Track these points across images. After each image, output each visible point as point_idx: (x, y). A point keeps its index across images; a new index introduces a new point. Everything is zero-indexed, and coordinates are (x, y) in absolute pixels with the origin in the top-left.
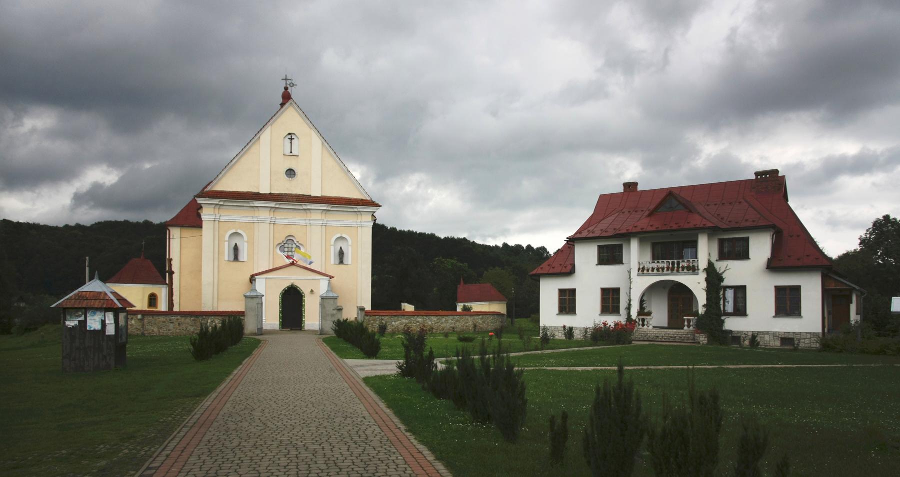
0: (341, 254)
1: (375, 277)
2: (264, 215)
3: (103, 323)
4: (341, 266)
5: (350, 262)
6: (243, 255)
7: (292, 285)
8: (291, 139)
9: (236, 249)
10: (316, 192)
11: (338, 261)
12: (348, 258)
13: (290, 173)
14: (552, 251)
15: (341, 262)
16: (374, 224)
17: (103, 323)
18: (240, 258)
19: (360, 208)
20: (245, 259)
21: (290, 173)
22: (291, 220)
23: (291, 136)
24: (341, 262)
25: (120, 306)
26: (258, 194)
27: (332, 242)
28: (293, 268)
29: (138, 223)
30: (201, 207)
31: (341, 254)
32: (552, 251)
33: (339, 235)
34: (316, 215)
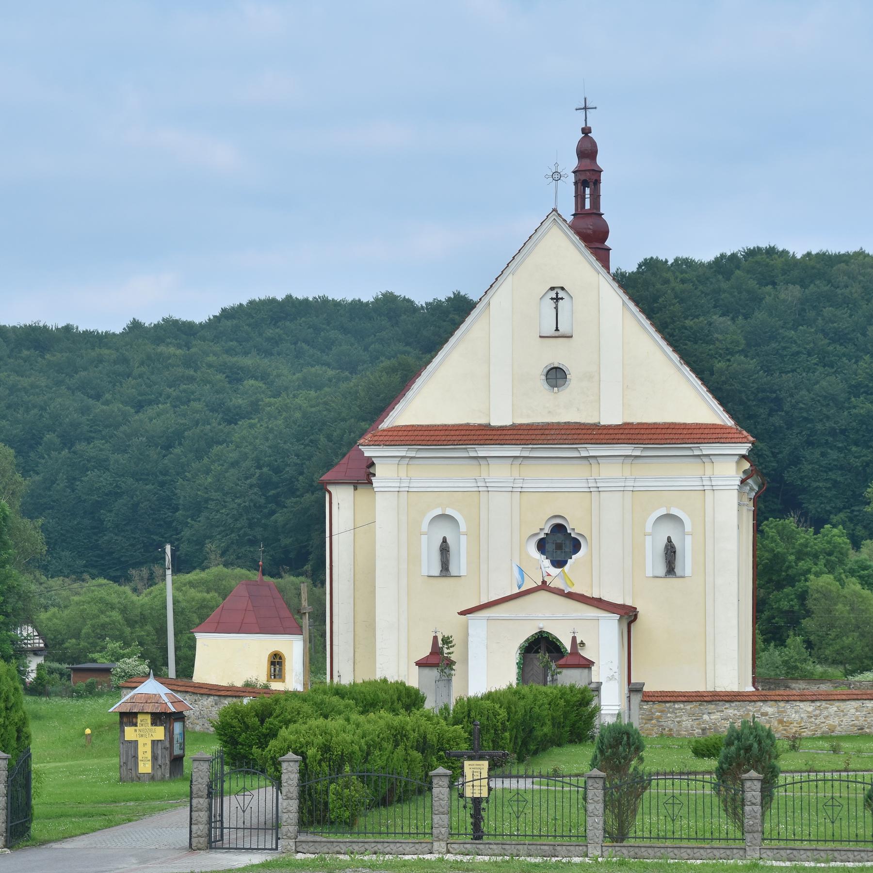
0: (670, 553)
2: (499, 474)
3: (276, 661)
4: (672, 581)
5: (688, 572)
6: (460, 563)
7: (541, 632)
8: (557, 299)
9: (444, 549)
11: (661, 569)
12: (687, 562)
15: (671, 570)
16: (184, 722)
17: (276, 661)
18: (453, 570)
20: (463, 572)
21: (556, 376)
23: (557, 294)
24: (671, 570)
25: (173, 710)
26: (487, 428)
28: (543, 595)
29: (357, 307)
31: (670, 553)
33: (663, 511)
34: (613, 468)
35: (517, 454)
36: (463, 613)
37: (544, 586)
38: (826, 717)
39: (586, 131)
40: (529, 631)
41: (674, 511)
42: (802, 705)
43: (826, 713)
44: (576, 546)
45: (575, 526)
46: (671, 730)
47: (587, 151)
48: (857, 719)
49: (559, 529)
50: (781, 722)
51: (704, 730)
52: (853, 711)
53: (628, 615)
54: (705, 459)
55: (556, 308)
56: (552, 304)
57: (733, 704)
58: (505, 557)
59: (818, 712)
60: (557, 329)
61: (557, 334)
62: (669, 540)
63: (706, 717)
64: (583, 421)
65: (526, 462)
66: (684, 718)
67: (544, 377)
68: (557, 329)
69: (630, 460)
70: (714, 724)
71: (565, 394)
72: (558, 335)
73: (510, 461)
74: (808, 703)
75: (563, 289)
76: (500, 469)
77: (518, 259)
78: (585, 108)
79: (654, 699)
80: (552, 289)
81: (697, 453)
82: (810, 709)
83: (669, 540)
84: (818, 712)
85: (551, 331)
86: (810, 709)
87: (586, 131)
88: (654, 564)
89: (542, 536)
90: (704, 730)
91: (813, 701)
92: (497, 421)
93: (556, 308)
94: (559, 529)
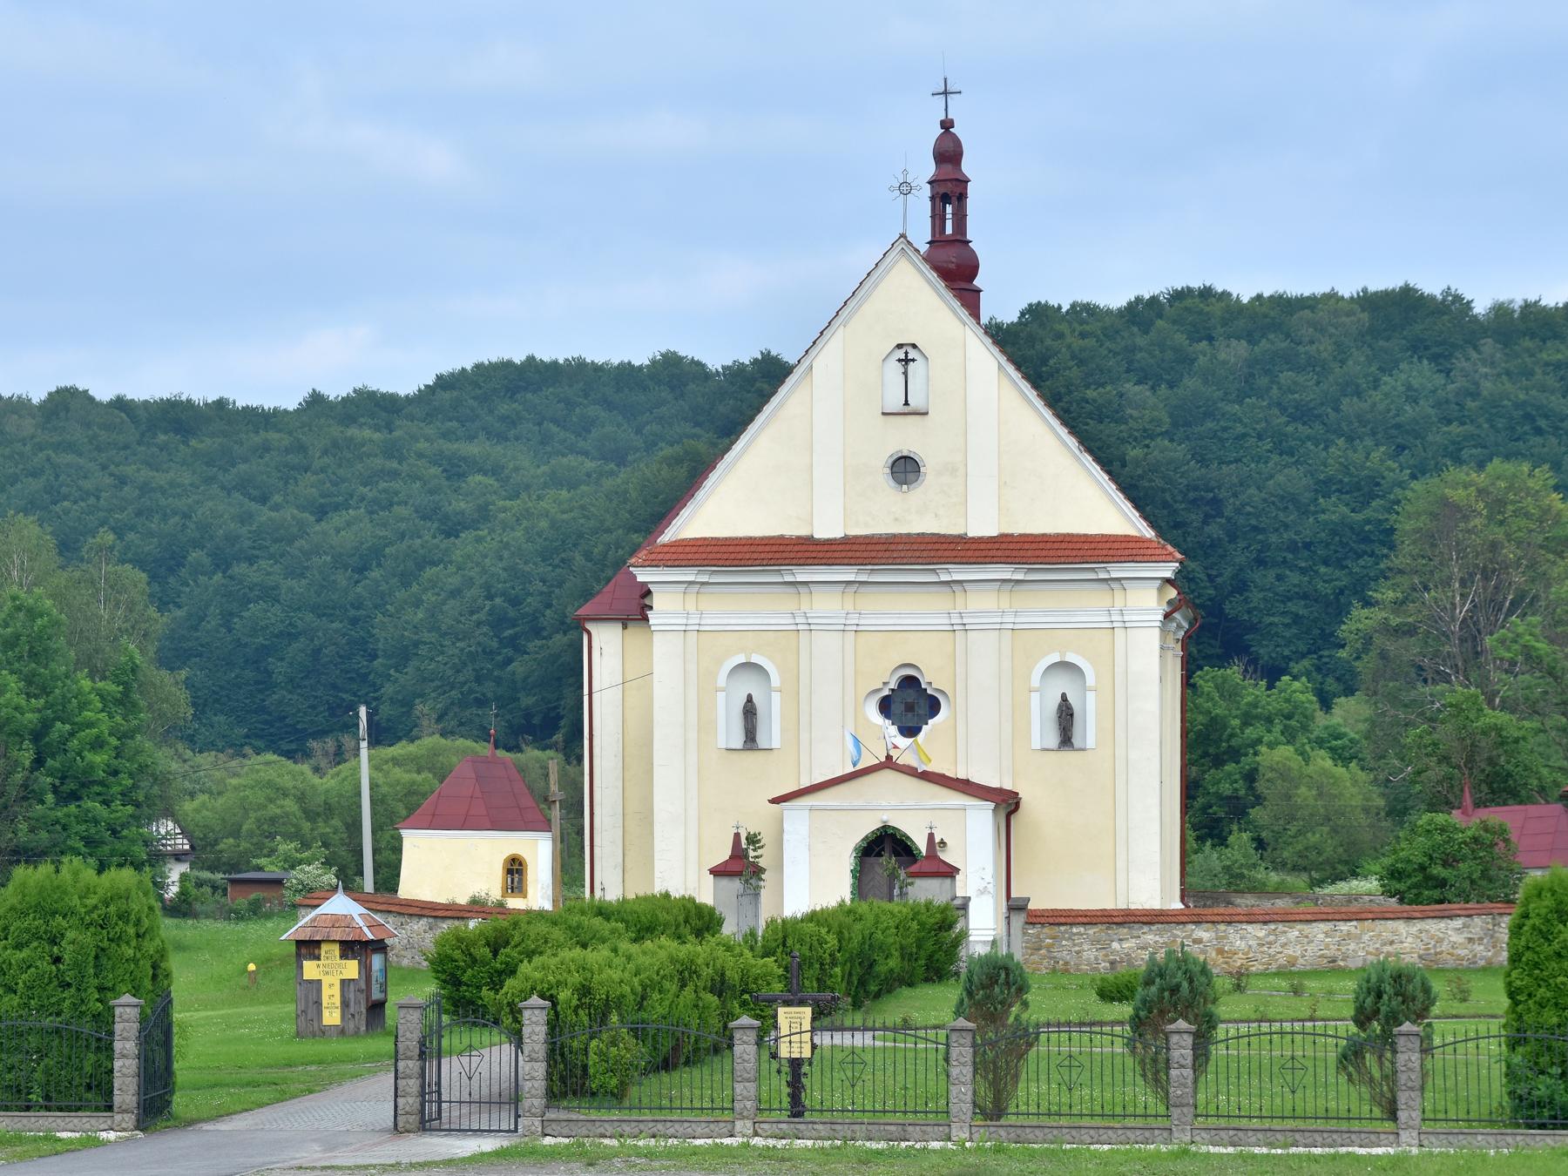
0: (1066, 716)
1: (1009, 350)
2: (826, 606)
3: (515, 869)
4: (1068, 756)
6: (772, 731)
8: (906, 361)
9: (750, 711)
10: (983, 526)
11: (1053, 739)
12: (1089, 729)
13: (905, 469)
14: (35, 401)
15: (1066, 740)
17: (515, 869)
18: (762, 740)
19: (1117, 571)
21: (905, 469)
22: (907, 624)
23: (906, 354)
24: (1066, 740)
26: (809, 541)
27: (1035, 681)
28: (888, 775)
30: (649, 593)
31: (1066, 716)
32: (35, 401)
34: (985, 598)
35: (851, 578)
36: (776, 801)
37: (889, 763)
38: (1284, 945)
39: (947, 125)
40: (868, 826)
41: (1071, 658)
42: (1249, 928)
43: (1283, 939)
44: (934, 706)
45: (932, 679)
46: (1066, 963)
47: (948, 153)
48: (1327, 947)
49: (910, 682)
50: (1220, 952)
51: (1112, 963)
52: (1321, 936)
53: (1007, 804)
54: (1115, 585)
55: (905, 374)
56: (899, 368)
57: (1154, 928)
58: (833, 721)
59: (1272, 938)
60: (906, 403)
61: (906, 409)
62: (1064, 697)
63: (1115, 945)
64: (943, 532)
65: (863, 589)
66: (1086, 947)
67: (888, 471)
68: (906, 403)
69: (1008, 586)
70: (1128, 955)
71: (917, 495)
72: (907, 410)
73: (840, 588)
74: (1259, 926)
75: (914, 346)
76: (827, 600)
77: (851, 304)
78: (946, 93)
79: (1043, 920)
80: (900, 346)
81: (1103, 575)
82: (1262, 934)
83: (1064, 697)
84: (1272, 938)
85: (896, 403)
86: (1262, 934)
87: (947, 125)
88: (1043, 731)
89: (886, 692)
90: (1112, 963)
91: (1265, 923)
92: (821, 533)
93: (905, 374)
94: (910, 682)
